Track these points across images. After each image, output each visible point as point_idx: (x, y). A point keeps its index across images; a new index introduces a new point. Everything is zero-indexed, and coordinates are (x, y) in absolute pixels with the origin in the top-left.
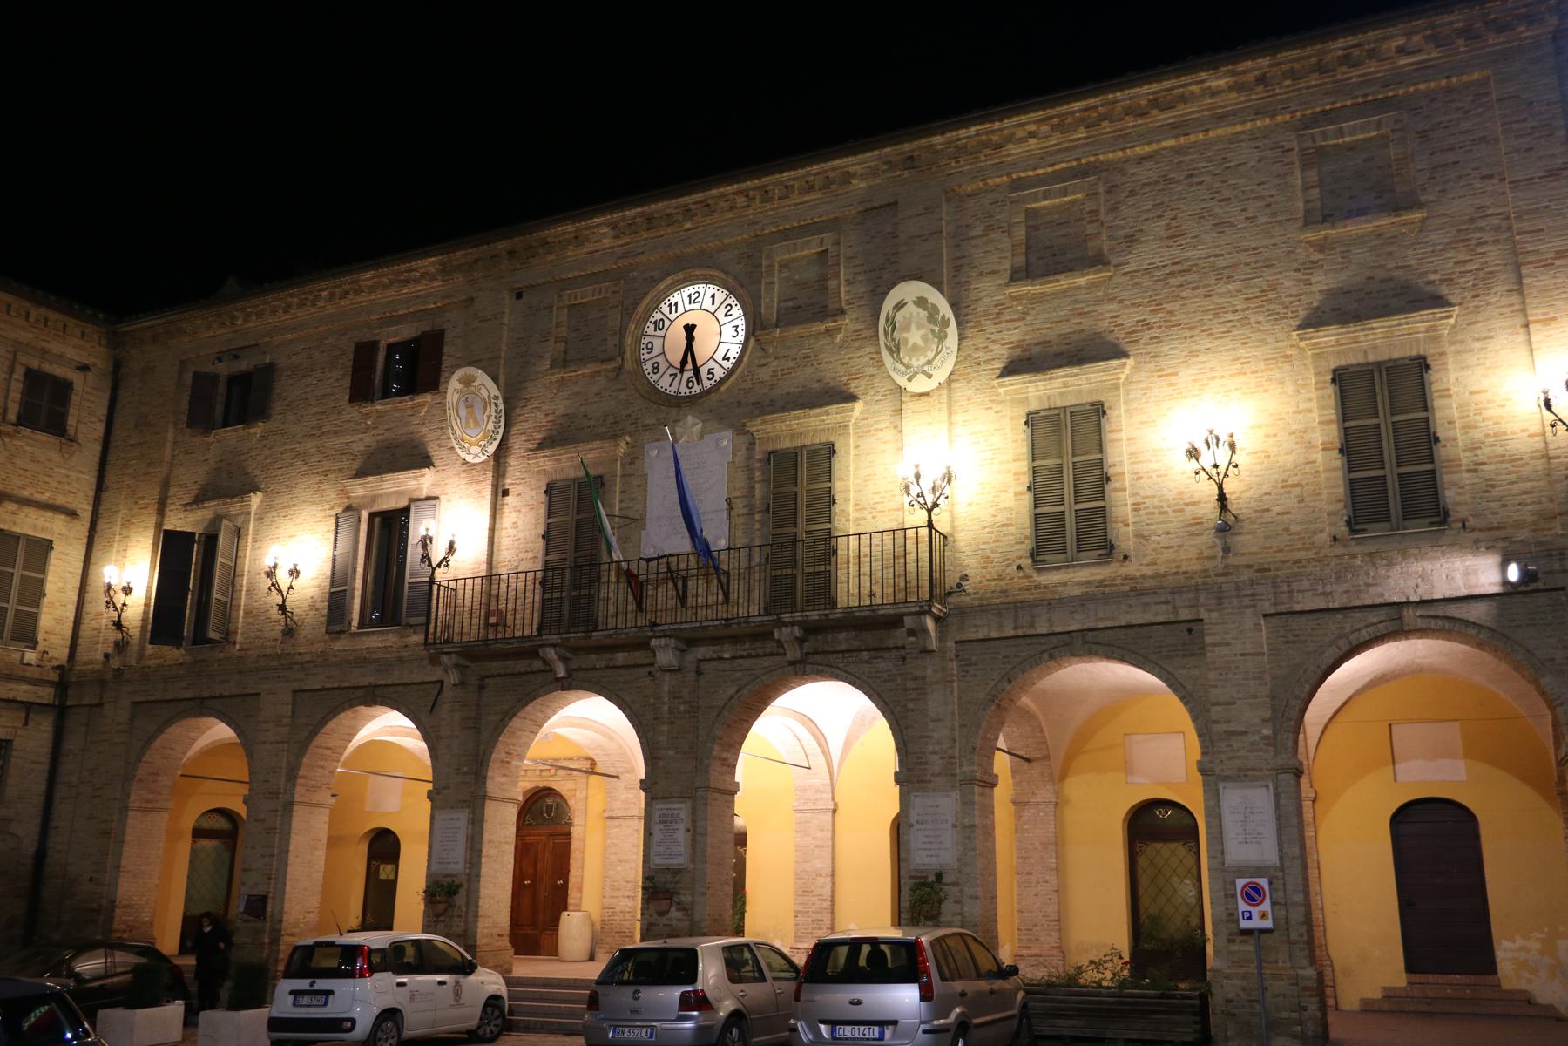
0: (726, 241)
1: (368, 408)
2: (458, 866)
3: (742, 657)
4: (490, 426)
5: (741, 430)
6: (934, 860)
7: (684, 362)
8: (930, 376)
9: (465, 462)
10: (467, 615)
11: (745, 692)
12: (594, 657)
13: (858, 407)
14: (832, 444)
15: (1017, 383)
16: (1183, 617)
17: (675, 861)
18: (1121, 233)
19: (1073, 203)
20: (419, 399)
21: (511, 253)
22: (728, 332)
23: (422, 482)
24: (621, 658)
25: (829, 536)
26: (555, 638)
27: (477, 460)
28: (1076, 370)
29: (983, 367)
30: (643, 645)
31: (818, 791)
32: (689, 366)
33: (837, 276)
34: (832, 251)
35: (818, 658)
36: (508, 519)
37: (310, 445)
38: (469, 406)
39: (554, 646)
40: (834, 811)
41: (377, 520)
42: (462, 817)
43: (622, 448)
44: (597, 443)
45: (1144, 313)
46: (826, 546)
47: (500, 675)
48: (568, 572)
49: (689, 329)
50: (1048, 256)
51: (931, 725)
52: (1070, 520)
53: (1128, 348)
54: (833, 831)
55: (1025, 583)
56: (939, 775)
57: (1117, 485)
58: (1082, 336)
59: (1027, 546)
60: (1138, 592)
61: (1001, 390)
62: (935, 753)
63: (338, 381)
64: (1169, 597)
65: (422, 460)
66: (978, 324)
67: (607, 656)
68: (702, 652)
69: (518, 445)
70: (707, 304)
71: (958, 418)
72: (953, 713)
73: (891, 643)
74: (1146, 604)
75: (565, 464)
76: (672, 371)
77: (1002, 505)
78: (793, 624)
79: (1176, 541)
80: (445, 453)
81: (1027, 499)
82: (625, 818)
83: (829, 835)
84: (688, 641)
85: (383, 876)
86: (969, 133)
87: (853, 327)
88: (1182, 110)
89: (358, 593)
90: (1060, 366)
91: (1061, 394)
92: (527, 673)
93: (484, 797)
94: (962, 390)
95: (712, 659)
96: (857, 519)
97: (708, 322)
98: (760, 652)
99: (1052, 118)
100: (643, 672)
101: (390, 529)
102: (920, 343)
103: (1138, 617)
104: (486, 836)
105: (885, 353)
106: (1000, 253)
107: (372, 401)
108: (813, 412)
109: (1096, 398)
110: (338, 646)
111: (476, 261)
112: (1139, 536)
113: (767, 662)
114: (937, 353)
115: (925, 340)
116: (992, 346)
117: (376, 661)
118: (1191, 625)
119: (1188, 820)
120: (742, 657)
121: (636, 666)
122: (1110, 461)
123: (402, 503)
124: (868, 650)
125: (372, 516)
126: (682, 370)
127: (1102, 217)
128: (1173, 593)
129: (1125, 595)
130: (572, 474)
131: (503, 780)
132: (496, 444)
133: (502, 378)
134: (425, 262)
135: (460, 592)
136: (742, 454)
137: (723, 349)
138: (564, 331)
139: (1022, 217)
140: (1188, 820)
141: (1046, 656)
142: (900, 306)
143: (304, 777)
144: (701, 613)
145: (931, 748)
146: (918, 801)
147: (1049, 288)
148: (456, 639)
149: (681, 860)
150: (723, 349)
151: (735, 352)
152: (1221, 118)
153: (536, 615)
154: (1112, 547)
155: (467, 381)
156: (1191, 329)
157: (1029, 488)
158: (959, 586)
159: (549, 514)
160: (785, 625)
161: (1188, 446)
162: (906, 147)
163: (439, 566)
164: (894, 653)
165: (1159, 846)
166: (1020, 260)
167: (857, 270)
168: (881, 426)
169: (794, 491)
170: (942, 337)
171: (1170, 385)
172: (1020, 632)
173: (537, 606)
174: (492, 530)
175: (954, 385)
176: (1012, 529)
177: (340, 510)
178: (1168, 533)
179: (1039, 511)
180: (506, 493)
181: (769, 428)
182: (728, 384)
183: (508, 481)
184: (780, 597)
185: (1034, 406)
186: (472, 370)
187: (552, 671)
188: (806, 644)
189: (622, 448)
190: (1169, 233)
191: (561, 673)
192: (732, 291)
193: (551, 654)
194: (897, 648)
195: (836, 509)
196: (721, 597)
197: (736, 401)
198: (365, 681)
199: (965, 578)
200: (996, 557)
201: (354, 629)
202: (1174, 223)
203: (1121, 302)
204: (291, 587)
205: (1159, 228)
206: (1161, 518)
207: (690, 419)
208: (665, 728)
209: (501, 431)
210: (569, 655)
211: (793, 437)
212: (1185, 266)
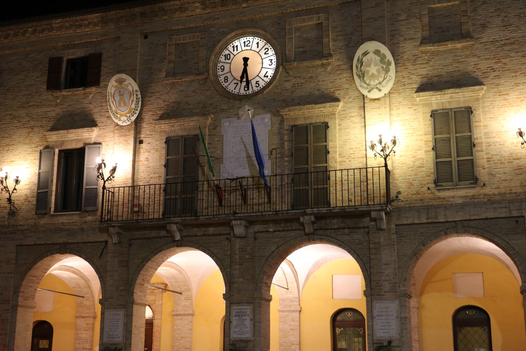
0: (265, 15)
1: (58, 94)
2: (118, 337)
3: (279, 231)
4: (133, 106)
5: (276, 113)
6: (386, 335)
7: (242, 77)
8: (380, 90)
9: (117, 125)
10: (120, 207)
11: (281, 249)
12: (196, 229)
13: (341, 104)
14: (327, 123)
15: (426, 96)
16: (514, 215)
17: (245, 336)
18: (479, 22)
19: (453, 6)
20: (88, 90)
21: (142, 14)
22: (266, 63)
23: (92, 135)
24: (211, 230)
26: (178, 219)
27: (125, 124)
28: (458, 90)
30: (228, 224)
31: (291, 301)
32: (245, 80)
33: (328, 36)
34: (325, 23)
35: (320, 232)
36: (143, 156)
37: (22, 112)
38: (121, 95)
39: (176, 223)
40: (300, 311)
41: (63, 154)
42: (121, 314)
43: (209, 121)
44: (196, 118)
45: (491, 63)
46: (325, 174)
47: (141, 239)
48: (179, 185)
49: (246, 60)
50: (441, 32)
51: (384, 267)
52: (455, 165)
53: (483, 80)
54: (300, 322)
55: (432, 196)
56: (388, 292)
57: (479, 149)
58: (459, 73)
59: (433, 177)
60: (491, 202)
61: (418, 99)
62: (386, 281)
63: (40, 79)
64: (507, 205)
65: (92, 124)
66: (404, 65)
67: (204, 229)
68: (257, 228)
69: (148, 117)
70: (254, 47)
71: (394, 112)
72: (395, 261)
73: (361, 225)
74: (495, 208)
75: (177, 128)
76: (235, 81)
77: (418, 157)
78: (311, 214)
79: (509, 177)
80: (104, 119)
81: (432, 154)
82: (184, 315)
83: (298, 324)
84: (250, 222)
85: (41, 346)
89: (54, 193)
90: (449, 88)
91: (449, 102)
92: (157, 237)
93: (133, 303)
94: (396, 98)
95: (263, 232)
96: (340, 162)
97: (256, 57)
98: (290, 228)
100: (223, 238)
101: (72, 161)
102: (376, 73)
103: (491, 214)
104: (134, 323)
105: (356, 77)
106: (416, 30)
107: (61, 91)
108: (317, 106)
109: (467, 105)
110: (42, 221)
111: (122, 17)
112: (490, 174)
113: (292, 234)
114: (384, 79)
115: (378, 71)
116: (411, 77)
117: (67, 230)
118: (518, 219)
119: (360, 318)
121: (220, 234)
122: (475, 136)
123: (80, 145)
124: (348, 228)
125: (60, 151)
126: (241, 81)
127: (469, 14)
128: (509, 203)
129: (485, 203)
130: (180, 133)
131: (140, 294)
132: (135, 116)
133: (137, 80)
134: (92, 16)
135: (116, 195)
136: (276, 126)
137: (264, 71)
138: (173, 57)
139: (426, 12)
140: (360, 318)
141: (443, 233)
142: (365, 54)
143: (23, 292)
144: (256, 208)
145: (384, 278)
146: (377, 305)
147: (441, 48)
148: (114, 219)
149: (248, 335)
150: (264, 71)
151: (271, 73)
153: (161, 207)
154: (477, 179)
155: (120, 82)
156: (516, 72)
157: (433, 149)
158: (397, 197)
159: (168, 154)
160: (307, 215)
161: (518, 130)
163: (107, 180)
164: (362, 230)
165: (468, 329)
166: (426, 33)
167: (337, 34)
168: (353, 114)
169: (308, 147)
170: (387, 71)
171: (505, 100)
172: (430, 221)
173: (162, 202)
174: (134, 161)
175: (392, 95)
176: (424, 169)
177: (42, 148)
178: (505, 173)
179: (438, 160)
180: (141, 142)
181: (292, 113)
182: (268, 90)
183: (142, 136)
184: (300, 201)
185: (435, 108)
186: (124, 76)
187: (173, 237)
188: (315, 225)
189: (209, 121)
190: (504, 24)
191: (178, 237)
192: (268, 41)
193: (174, 227)
194: (364, 228)
195: (330, 156)
196: (266, 200)
197: (272, 98)
198: (61, 241)
199: (399, 193)
200: (416, 183)
201: (52, 212)
202: (506, 19)
203: (479, 57)
204: (15, 189)
205: (498, 21)
206: (501, 166)
207: (247, 107)
208: (238, 267)
209: (139, 109)
210: (183, 229)
211: (305, 118)
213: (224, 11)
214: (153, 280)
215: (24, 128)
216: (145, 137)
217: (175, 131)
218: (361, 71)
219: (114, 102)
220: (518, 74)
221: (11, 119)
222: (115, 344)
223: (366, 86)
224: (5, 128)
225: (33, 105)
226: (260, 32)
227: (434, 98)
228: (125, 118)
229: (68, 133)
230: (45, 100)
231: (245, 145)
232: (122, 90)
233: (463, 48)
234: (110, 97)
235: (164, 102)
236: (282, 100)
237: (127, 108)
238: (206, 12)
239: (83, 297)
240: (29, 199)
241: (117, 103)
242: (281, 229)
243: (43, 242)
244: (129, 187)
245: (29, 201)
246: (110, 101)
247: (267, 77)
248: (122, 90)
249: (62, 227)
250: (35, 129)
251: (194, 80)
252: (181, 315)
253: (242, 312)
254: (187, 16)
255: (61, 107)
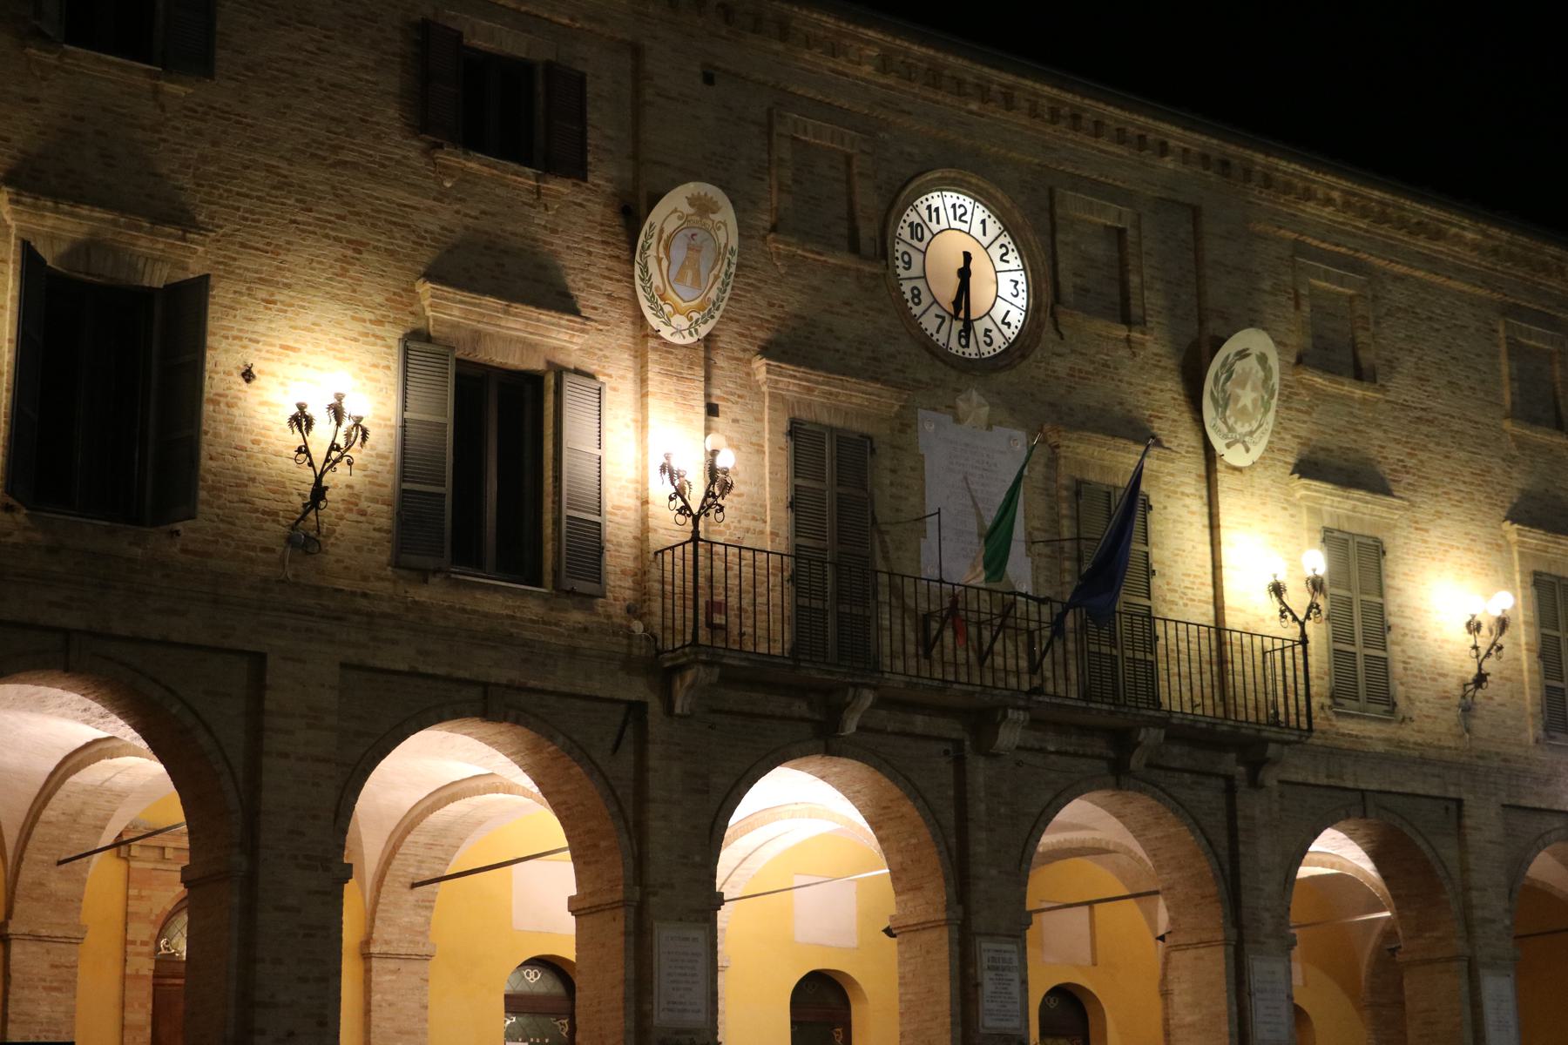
4: (713, 295)
19: (1339, 294)
24: (920, 722)
25: (1149, 617)
27: (677, 340)
29: (1277, 455)
44: (875, 387)
86: (1287, 167)
87: (1156, 349)
88: (1440, 246)
91: (1348, 517)
92: (783, 718)
99: (1355, 195)
120: (1066, 753)
124: (1191, 772)
141: (1343, 812)
142: (1242, 354)
151: (1017, 318)
152: (1459, 271)
154: (1395, 704)
155: (703, 207)
156: (1437, 487)
162: (1232, 149)
195: (1156, 581)
203: (1385, 431)
208: (983, 835)
212: (1431, 416)
213: (925, 99)
214: (1040, 849)
215: (327, 236)
216: (727, 400)
217: (809, 405)
218: (1224, 391)
219: (665, 263)
220: (1439, 491)
221: (274, 188)
222: (689, 1032)
223: (1225, 430)
224: (252, 212)
225: (355, 165)
226: (999, 195)
227: (1328, 500)
228: (685, 323)
229: (506, 312)
230: (398, 162)
231: (973, 498)
232: (701, 235)
233: (1364, 401)
234: (654, 241)
235: (771, 305)
236: (1051, 404)
237: (697, 293)
238: (882, 81)
239: (60, 863)
240: (364, 504)
241: (674, 270)
242: (1071, 749)
243: (441, 671)
244: (683, 544)
245: (363, 513)
246: (652, 252)
247: (1009, 325)
248: (701, 235)
249: (513, 630)
250: (365, 255)
251: (848, 269)
252: (397, 957)
253: (1004, 960)
254: (832, 71)
255: (457, 207)
